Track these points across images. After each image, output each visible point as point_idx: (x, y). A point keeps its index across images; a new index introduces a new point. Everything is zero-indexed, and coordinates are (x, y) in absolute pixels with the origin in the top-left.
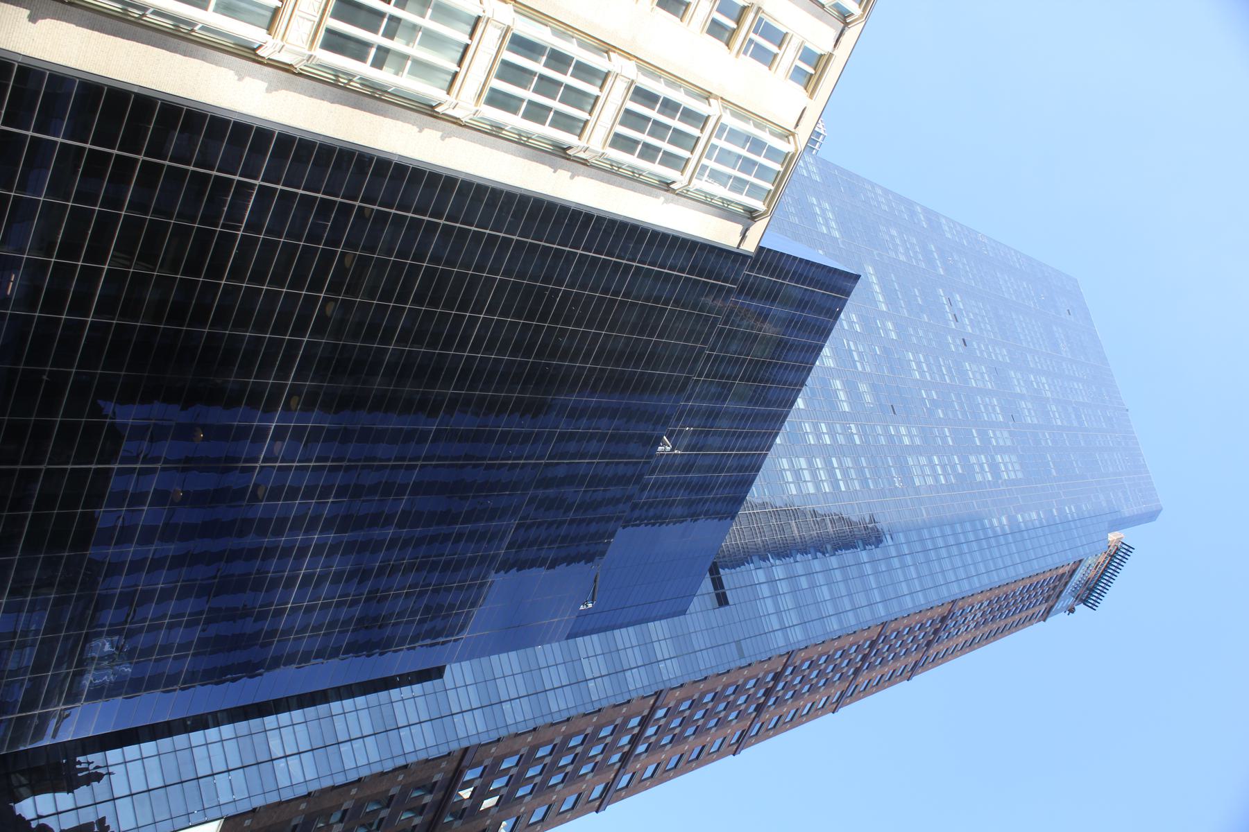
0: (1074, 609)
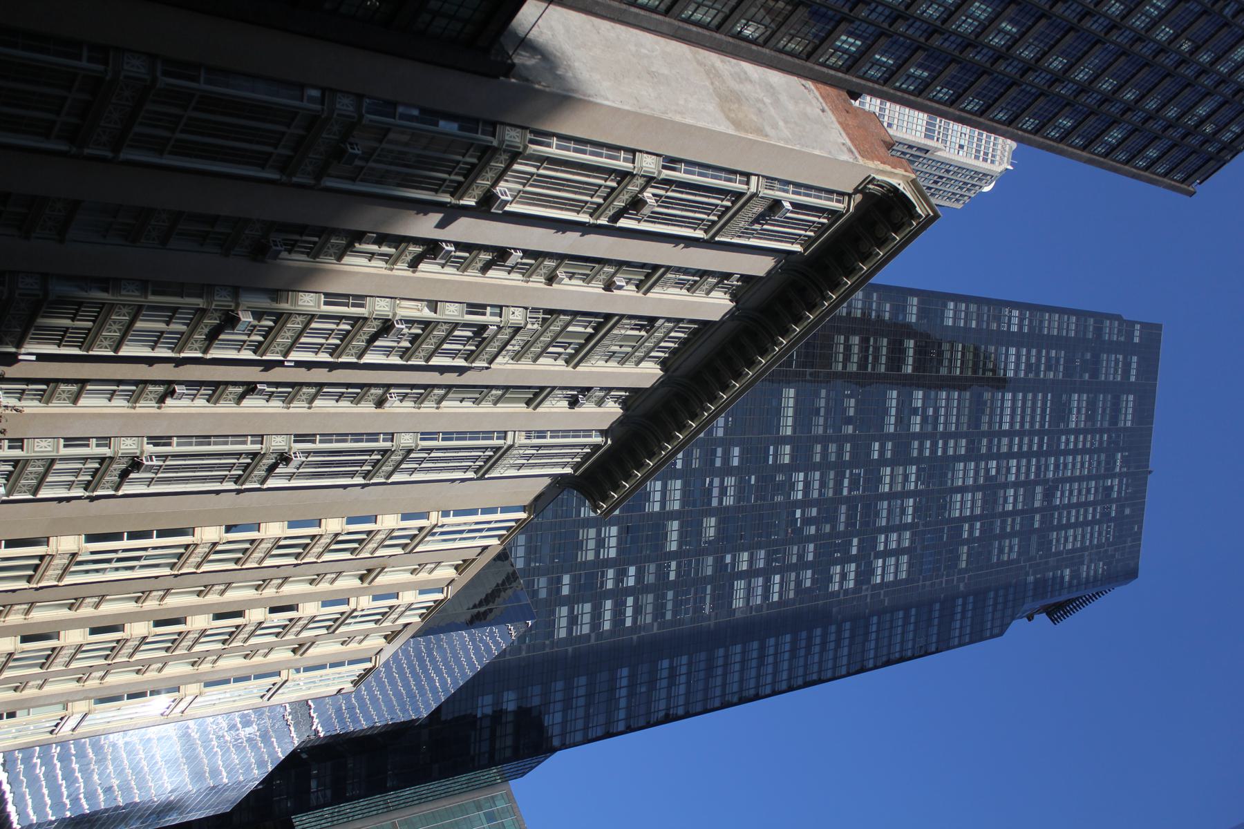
0: (1033, 618)
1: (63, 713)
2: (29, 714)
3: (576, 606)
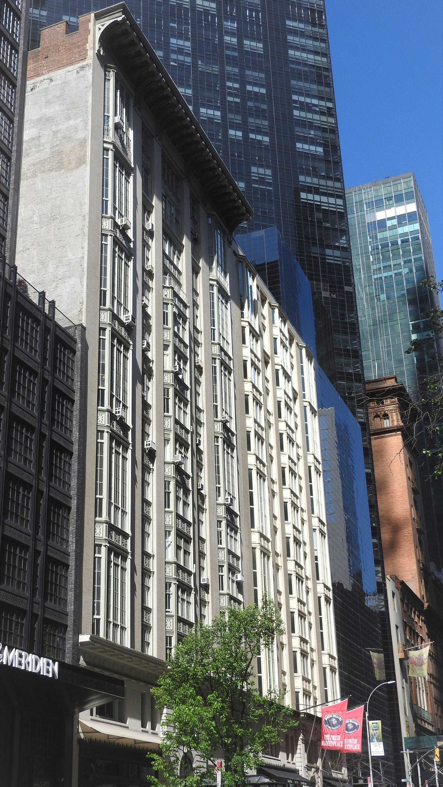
1: (318, 532)
2: (317, 550)
3: (253, 178)
